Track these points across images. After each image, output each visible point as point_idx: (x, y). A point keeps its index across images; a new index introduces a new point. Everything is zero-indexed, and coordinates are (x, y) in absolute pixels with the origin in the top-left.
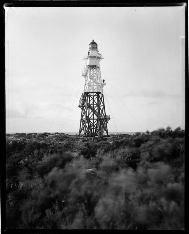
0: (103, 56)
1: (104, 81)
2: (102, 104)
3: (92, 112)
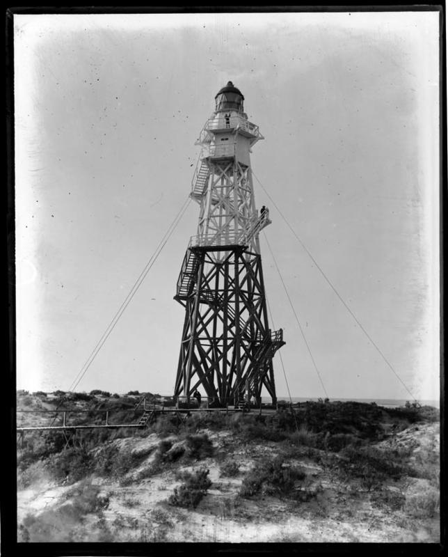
0: (262, 132)
1: (263, 210)
2: (256, 291)
3: (245, 269)
